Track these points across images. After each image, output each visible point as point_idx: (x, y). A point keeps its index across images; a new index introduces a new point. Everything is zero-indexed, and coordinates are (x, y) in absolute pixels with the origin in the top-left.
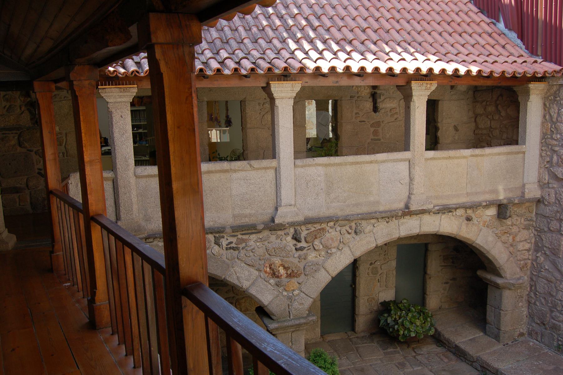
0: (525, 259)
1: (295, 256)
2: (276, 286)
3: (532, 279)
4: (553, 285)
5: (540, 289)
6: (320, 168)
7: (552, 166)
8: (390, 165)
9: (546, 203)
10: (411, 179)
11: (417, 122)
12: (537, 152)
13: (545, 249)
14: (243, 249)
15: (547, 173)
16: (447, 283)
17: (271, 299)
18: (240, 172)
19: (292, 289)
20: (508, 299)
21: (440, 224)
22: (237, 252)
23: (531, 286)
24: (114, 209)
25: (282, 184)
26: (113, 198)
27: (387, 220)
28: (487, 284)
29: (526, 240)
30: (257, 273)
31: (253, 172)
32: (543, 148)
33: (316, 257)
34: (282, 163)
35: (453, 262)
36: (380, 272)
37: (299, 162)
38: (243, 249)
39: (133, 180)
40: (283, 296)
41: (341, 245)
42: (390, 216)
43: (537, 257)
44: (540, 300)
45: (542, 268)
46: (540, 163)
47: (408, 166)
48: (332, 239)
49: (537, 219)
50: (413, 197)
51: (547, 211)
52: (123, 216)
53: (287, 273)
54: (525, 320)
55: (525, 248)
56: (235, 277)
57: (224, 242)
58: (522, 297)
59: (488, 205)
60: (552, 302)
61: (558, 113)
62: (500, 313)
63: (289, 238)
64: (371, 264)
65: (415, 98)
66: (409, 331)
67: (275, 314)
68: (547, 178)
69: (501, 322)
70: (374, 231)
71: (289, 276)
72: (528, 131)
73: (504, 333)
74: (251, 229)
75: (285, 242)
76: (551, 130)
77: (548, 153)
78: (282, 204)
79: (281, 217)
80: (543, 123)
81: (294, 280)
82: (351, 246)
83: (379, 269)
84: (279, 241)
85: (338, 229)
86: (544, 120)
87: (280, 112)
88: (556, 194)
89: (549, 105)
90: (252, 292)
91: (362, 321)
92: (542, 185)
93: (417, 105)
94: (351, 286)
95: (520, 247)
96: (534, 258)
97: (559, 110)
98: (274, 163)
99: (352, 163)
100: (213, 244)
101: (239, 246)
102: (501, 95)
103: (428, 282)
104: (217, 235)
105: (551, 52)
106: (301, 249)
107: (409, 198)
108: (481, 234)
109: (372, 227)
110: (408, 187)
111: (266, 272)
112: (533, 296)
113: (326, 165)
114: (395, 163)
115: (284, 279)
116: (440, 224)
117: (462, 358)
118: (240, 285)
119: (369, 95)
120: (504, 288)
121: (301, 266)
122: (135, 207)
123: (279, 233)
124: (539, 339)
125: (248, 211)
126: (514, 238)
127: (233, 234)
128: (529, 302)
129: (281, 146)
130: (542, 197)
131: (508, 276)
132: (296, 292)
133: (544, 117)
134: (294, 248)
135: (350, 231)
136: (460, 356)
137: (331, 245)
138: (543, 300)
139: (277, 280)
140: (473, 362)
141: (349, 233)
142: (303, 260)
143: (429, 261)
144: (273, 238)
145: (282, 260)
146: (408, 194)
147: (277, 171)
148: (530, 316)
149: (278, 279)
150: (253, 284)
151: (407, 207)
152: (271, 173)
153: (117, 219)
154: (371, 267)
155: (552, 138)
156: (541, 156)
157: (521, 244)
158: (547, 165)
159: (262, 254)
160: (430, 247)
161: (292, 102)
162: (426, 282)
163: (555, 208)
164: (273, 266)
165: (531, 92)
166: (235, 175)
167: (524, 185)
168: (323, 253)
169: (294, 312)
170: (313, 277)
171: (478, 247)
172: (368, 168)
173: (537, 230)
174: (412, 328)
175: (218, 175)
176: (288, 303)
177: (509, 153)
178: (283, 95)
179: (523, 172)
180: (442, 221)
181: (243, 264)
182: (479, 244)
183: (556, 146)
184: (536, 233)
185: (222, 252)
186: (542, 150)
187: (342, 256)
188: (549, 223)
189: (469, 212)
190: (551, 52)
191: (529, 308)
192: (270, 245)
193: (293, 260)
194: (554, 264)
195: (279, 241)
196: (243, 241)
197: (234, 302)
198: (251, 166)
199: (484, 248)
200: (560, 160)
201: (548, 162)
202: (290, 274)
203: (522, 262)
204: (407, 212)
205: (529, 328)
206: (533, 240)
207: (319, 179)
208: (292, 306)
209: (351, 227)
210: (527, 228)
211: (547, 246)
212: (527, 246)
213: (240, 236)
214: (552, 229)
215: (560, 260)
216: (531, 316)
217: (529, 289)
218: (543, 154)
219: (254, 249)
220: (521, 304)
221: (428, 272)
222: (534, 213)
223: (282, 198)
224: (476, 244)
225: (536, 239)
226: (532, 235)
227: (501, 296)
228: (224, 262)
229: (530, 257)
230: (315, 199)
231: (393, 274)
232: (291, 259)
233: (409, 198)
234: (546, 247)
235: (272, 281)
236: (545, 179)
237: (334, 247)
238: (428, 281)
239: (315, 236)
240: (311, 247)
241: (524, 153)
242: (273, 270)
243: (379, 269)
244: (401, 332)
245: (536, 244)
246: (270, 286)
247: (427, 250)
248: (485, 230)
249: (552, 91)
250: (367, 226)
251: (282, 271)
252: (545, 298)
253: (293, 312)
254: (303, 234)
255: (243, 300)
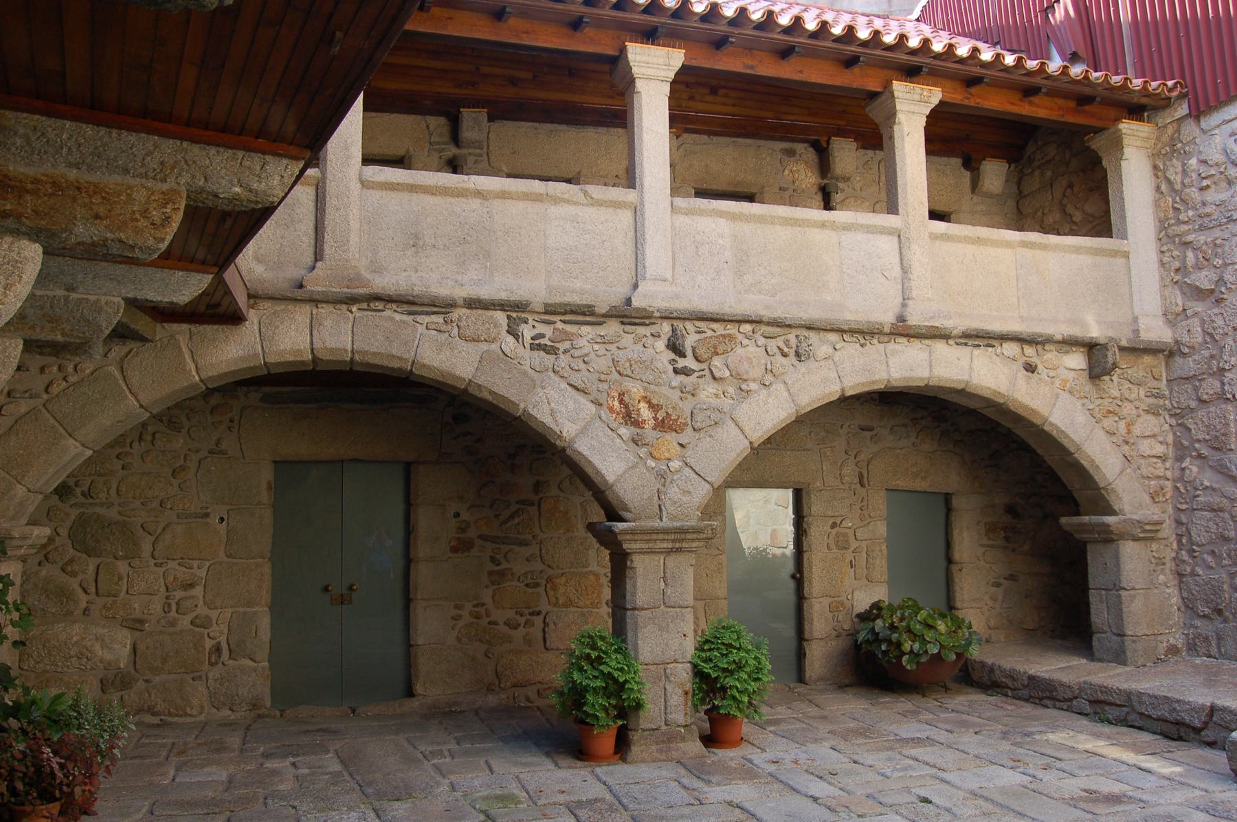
0: (1159, 477)
1: (674, 384)
2: (632, 445)
3: (1179, 523)
4: (1226, 515)
5: (1199, 535)
6: (722, 221)
7: (1187, 274)
8: (860, 237)
9: (1186, 350)
10: (905, 270)
11: (908, 161)
12: (1153, 257)
13: (1197, 445)
14: (565, 352)
15: (1178, 292)
16: (998, 585)
17: (620, 472)
18: (566, 205)
19: (667, 455)
20: (1133, 561)
21: (971, 368)
22: (552, 357)
23: (1179, 536)
24: (313, 242)
25: (647, 237)
26: (313, 218)
27: (862, 341)
28: (1085, 543)
29: (1154, 436)
30: (593, 408)
31: (591, 211)
32: (1165, 248)
33: (717, 396)
34: (648, 197)
35: (1007, 539)
36: (854, 545)
37: (680, 202)
38: (565, 352)
39: (355, 186)
40: (647, 468)
41: (769, 378)
42: (865, 333)
43: (1183, 469)
44: (1204, 560)
45: (1196, 489)
46: (1162, 278)
47: (896, 246)
48: (750, 360)
49: (1171, 392)
50: (910, 302)
51: (1188, 366)
52: (328, 251)
53: (655, 419)
54: (1177, 617)
55: (1154, 452)
56: (546, 409)
57: (527, 332)
58: (1164, 564)
59: (1070, 343)
60: (1229, 555)
61: (1184, 171)
62: (1120, 596)
63: (661, 345)
64: (834, 525)
65: (900, 117)
66: (924, 641)
67: (631, 505)
68: (1179, 301)
69: (1125, 617)
70: (836, 359)
71: (663, 425)
72: (1128, 214)
73: (1134, 642)
74: (583, 313)
75: (651, 350)
76: (1175, 209)
77: (1176, 253)
78: (648, 276)
79: (645, 296)
80: (1157, 204)
81: (671, 437)
82: (790, 382)
83: (852, 538)
84: (639, 347)
85: (762, 341)
86: (1158, 196)
87: (644, 103)
88: (1203, 322)
89: (1164, 164)
90: (580, 449)
91: (819, 656)
92: (1172, 318)
93: (906, 129)
94: (793, 577)
95: (1146, 447)
96: (1177, 474)
97: (1184, 165)
98: (630, 196)
99: (786, 222)
100: (504, 333)
101: (557, 345)
102: (1071, 186)
103: (957, 580)
104: (514, 315)
105: (1152, 61)
106: (686, 372)
107: (904, 305)
108: (1055, 401)
109: (831, 350)
110: (900, 287)
111: (611, 410)
112: (1186, 558)
113: (734, 217)
114: (871, 236)
115: (649, 433)
116: (971, 368)
117: (1046, 702)
118: (557, 430)
119: (815, 189)
120: (1122, 536)
121: (686, 407)
122: (354, 238)
123: (641, 330)
124: (1214, 651)
125: (578, 284)
126: (1128, 425)
127: (547, 317)
128: (1180, 575)
129: (646, 165)
130: (1177, 342)
131: (1127, 508)
132: (675, 464)
133: (1158, 188)
134: (671, 368)
135: (786, 350)
136: (1041, 699)
137: (747, 372)
138: (1209, 559)
139: (635, 430)
140: (1070, 700)
141: (785, 355)
142: (689, 396)
143: (956, 533)
144: (627, 340)
145: (645, 389)
146: (900, 299)
147: (637, 211)
148: (1187, 607)
149: (638, 430)
150: (584, 430)
151: (901, 318)
152: (626, 217)
153: (316, 260)
154: (834, 531)
155: (1179, 222)
156: (1162, 264)
157: (1147, 442)
158: (1177, 277)
159: (604, 369)
160: (955, 502)
161: (667, 89)
162: (953, 581)
163: (1206, 353)
164: (626, 398)
165: (1126, 141)
166: (554, 210)
167: (1135, 320)
168: (731, 390)
169: (671, 509)
170: (710, 436)
171: (1054, 433)
172: (816, 235)
173: (1176, 414)
174: (929, 635)
175: (521, 205)
176: (658, 486)
177: (1098, 252)
178: (650, 72)
179: (1131, 295)
180: (975, 362)
181: (564, 385)
182: (1057, 428)
183: (1188, 232)
184: (1174, 422)
185: (520, 350)
186: (1162, 252)
187: (770, 400)
188: (1196, 389)
189: (1029, 351)
190: (1152, 61)
191: (1181, 589)
192: (621, 352)
193: (669, 391)
194: (1222, 470)
195: (639, 347)
196: (568, 337)
197: (544, 582)
198: (585, 193)
199: (1067, 437)
200: (1200, 256)
201: (1177, 270)
202: (663, 420)
203: (1153, 483)
204: (903, 330)
205: (1187, 635)
206: (1170, 439)
207: (721, 241)
208: (666, 494)
209: (787, 342)
210: (1153, 411)
211: (1201, 437)
212: (1159, 449)
213: (560, 325)
214: (1205, 397)
215: (1232, 456)
216: (1188, 605)
217: (1175, 546)
218: (1166, 259)
219: (587, 355)
220: (1161, 577)
221: (956, 556)
222: (1165, 382)
223: (647, 265)
224: (1051, 424)
225: (1175, 434)
226: (1167, 427)
227: (1117, 557)
228: (525, 374)
229: (1169, 474)
230: (713, 279)
231: (881, 551)
232: (664, 390)
233: (904, 305)
234: (1199, 441)
235: (623, 431)
236: (1177, 305)
237: (754, 380)
238: (957, 578)
239: (715, 347)
240: (707, 372)
241: (1126, 255)
242: (626, 406)
243: (852, 538)
244: (907, 647)
245: (1178, 445)
246: (618, 441)
247: (949, 510)
248: (1065, 396)
249: (1166, 138)
250: (821, 345)
251: (645, 413)
252: (1213, 552)
253: (669, 508)
254: (690, 341)
255: (563, 580)
